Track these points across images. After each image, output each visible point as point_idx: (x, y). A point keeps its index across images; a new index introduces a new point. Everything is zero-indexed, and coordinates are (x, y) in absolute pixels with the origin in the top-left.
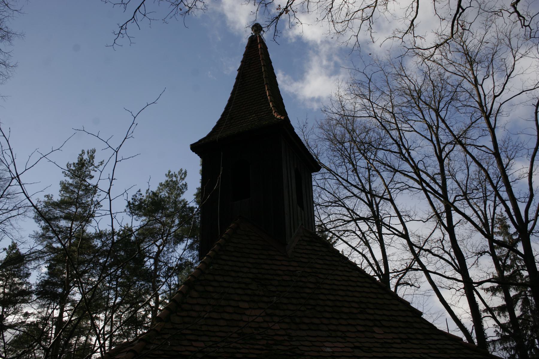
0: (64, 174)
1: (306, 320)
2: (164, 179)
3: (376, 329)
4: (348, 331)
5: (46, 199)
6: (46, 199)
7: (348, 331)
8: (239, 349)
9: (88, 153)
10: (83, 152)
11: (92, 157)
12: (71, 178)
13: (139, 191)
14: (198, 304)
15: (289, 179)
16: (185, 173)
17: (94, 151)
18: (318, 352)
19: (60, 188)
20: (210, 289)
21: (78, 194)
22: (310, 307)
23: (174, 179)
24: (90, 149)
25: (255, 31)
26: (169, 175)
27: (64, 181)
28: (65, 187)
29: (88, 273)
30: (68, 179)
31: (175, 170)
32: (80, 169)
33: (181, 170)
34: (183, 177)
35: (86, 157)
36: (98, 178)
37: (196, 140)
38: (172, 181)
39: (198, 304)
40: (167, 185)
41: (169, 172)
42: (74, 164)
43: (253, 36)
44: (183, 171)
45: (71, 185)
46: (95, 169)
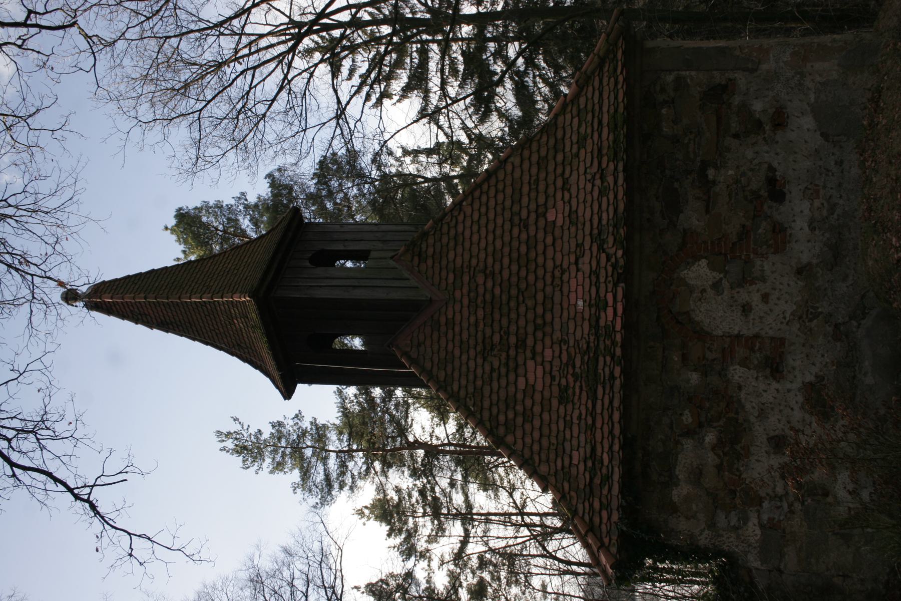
0: (260, 472)
1: (540, 310)
3: (551, 217)
5: (299, 491)
6: (299, 491)
7: (553, 259)
8: (580, 414)
9: (223, 441)
10: (223, 449)
11: (228, 435)
12: (264, 460)
15: (335, 282)
17: (219, 433)
18: (583, 319)
20: (502, 418)
22: (521, 298)
25: (76, 300)
27: (269, 470)
28: (279, 466)
29: (383, 400)
30: (265, 465)
32: (250, 451)
35: (230, 444)
37: (277, 392)
42: (244, 461)
43: (86, 306)
45: (274, 459)
46: (245, 427)
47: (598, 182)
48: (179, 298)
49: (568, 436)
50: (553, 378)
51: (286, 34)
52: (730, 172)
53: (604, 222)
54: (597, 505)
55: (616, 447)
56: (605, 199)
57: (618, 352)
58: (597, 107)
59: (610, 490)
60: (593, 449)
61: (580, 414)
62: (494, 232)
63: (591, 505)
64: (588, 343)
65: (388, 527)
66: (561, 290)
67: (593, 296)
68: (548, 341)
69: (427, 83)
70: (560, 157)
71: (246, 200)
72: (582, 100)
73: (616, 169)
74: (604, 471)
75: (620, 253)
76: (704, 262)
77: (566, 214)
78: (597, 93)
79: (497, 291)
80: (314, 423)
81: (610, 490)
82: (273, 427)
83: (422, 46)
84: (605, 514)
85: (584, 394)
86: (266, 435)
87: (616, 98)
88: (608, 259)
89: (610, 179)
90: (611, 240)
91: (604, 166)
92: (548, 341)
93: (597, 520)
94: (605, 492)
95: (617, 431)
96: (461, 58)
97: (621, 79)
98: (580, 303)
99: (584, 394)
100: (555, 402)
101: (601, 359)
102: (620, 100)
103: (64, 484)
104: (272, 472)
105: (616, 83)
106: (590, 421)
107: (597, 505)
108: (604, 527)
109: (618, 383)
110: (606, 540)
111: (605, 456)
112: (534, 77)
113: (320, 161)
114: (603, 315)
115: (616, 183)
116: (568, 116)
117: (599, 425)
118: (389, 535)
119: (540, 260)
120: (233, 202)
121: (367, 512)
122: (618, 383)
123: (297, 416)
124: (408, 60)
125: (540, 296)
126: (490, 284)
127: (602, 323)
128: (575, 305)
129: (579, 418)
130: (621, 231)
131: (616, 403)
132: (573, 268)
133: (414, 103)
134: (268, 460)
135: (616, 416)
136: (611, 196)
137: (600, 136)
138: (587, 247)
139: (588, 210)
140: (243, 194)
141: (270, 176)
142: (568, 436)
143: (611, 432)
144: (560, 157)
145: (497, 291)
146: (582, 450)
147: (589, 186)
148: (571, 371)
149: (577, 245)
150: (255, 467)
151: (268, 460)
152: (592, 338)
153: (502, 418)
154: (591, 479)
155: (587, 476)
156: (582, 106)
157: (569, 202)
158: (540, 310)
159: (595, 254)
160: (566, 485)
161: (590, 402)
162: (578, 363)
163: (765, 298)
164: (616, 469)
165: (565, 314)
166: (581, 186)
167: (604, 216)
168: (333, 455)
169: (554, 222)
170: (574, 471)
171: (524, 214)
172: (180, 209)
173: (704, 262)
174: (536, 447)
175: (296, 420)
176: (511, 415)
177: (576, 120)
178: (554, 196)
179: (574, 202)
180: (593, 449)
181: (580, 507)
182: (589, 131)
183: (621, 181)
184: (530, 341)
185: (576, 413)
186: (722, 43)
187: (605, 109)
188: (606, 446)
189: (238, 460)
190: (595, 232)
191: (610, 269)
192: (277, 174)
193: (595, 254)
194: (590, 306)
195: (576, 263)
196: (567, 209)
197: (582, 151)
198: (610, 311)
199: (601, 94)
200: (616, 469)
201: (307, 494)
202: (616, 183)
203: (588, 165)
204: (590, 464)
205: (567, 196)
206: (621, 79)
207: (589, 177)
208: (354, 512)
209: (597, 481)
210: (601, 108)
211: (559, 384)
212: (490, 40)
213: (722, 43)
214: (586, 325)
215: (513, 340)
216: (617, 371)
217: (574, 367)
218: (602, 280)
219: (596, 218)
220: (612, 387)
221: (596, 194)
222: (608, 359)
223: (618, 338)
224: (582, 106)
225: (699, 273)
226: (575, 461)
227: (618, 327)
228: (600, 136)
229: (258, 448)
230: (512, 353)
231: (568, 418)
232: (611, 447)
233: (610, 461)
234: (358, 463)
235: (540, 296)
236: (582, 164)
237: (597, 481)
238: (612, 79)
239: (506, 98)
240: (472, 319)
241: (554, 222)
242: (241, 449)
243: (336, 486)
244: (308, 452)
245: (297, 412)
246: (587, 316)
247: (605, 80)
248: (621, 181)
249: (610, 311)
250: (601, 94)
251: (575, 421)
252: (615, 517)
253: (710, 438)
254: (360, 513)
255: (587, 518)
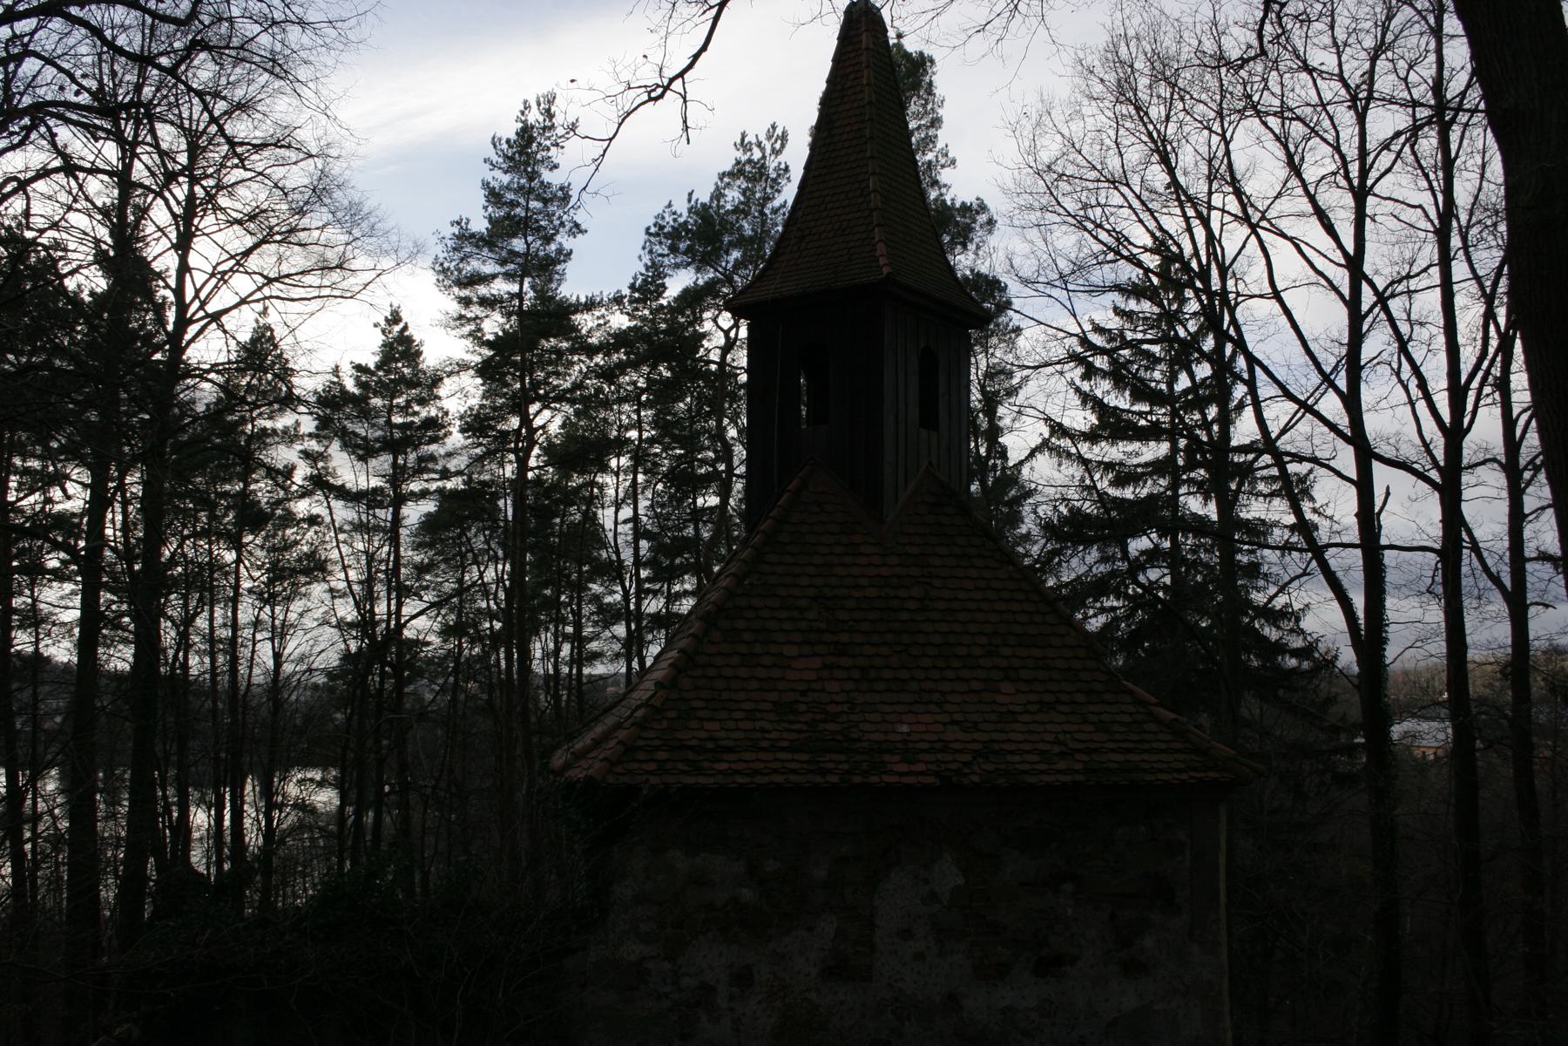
0: (488, 166)
1: (887, 674)
2: (728, 158)
3: (1006, 687)
4: (953, 691)
5: (456, 230)
7: (953, 691)
8: (768, 732)
9: (539, 104)
10: (527, 106)
11: (549, 114)
12: (506, 172)
13: (670, 205)
14: (719, 654)
16: (784, 138)
17: (551, 102)
18: (886, 733)
19: (483, 201)
20: (741, 624)
21: (522, 210)
23: (757, 154)
24: (544, 90)
26: (744, 145)
28: (494, 196)
30: (498, 174)
31: (757, 130)
33: (774, 127)
34: (778, 146)
35: (534, 117)
36: (567, 165)
38: (750, 161)
39: (719, 654)
40: (738, 172)
41: (743, 136)
44: (779, 131)
47: (1056, 749)
48: (873, 157)
49: (736, 715)
50: (804, 693)
51: (1208, 255)
52: (1070, 911)
53: (1009, 758)
54: (661, 755)
55: (740, 780)
56: (1035, 758)
57: (857, 779)
58: (1147, 746)
59: (683, 772)
60: (729, 750)
61: (768, 732)
62: (980, 610)
63: (658, 748)
64: (858, 740)
65: (372, 366)
66: (915, 702)
67: (919, 746)
68: (850, 685)
69: (1106, 439)
70: (1080, 698)
71: (943, 166)
72: (1153, 727)
73: (1076, 771)
74: (706, 764)
75: (976, 779)
76: (961, 881)
77: (1011, 708)
78: (1164, 746)
79: (904, 616)
80: (564, 255)
81: (683, 772)
82: (562, 189)
83: (1165, 431)
84: (652, 766)
85: (795, 736)
86: (547, 176)
87: (1161, 771)
88: (966, 764)
89: (1062, 765)
90: (990, 767)
91: (1078, 756)
92: (850, 685)
93: (641, 756)
94: (680, 766)
95: (759, 780)
96: (1144, 493)
97: (1184, 776)
98: (905, 729)
99: (795, 736)
100: (773, 696)
101: (842, 757)
102: (1160, 776)
103: (690, 66)
104: (486, 185)
105: (1179, 771)
106: (764, 744)
107: (661, 755)
108: (635, 766)
109: (819, 779)
110: (619, 769)
111: (723, 766)
112: (1113, 609)
113: (999, 282)
114: (897, 758)
115: (1059, 772)
116: (1132, 709)
117: (762, 756)
118: (359, 368)
119: (950, 674)
120: (940, 145)
121: (397, 328)
122: (819, 779)
123: (577, 225)
124: (1146, 408)
125: (904, 674)
126: (912, 605)
127: (886, 757)
128: (901, 722)
129: (763, 730)
130: (1002, 781)
131: (793, 778)
132: (945, 718)
133: (1081, 419)
134: (506, 179)
135: (779, 779)
136: (1042, 767)
137: (1113, 750)
138: (976, 736)
139: (1020, 737)
140: (953, 162)
141: (983, 208)
142: (736, 715)
143: (756, 772)
144: (1080, 698)
145: (904, 616)
146: (723, 734)
147: (1050, 738)
148: (818, 717)
149: (975, 723)
150: (495, 159)
151: (506, 179)
152: (865, 745)
153: (741, 624)
154: (691, 748)
155: (694, 743)
156: (1145, 726)
157: (1027, 712)
158: (887, 674)
159: (970, 746)
160: (672, 714)
161: (786, 744)
162: (831, 727)
163: (919, 957)
164: (711, 780)
165: (887, 708)
166: (1048, 727)
167: (1017, 758)
168: (515, 288)
169: (999, 692)
170: (694, 724)
171: (1006, 651)
172: (932, 61)
173: (961, 881)
174: (711, 672)
175: (568, 226)
176: (747, 636)
177: (1127, 719)
178: (1031, 691)
179: (1027, 718)
180: (729, 750)
181: (652, 734)
182: (1118, 737)
183: (1062, 778)
184: (845, 661)
185: (768, 726)
186: (1223, 898)
187: (1146, 757)
188: (739, 766)
189: (510, 130)
190: (996, 747)
191: (954, 766)
192: (982, 218)
193: (970, 746)
194: (905, 741)
195: (953, 722)
196: (1018, 709)
197: (1091, 728)
198: (904, 768)
199: (1163, 751)
200: (711, 780)
201: (450, 243)
202: (1059, 772)
203: (1076, 736)
204: (710, 745)
205: (1033, 708)
206: (1184, 776)
207: (1061, 737)
208: (395, 305)
209: (691, 755)
210: (1146, 751)
211: (797, 702)
212: (1174, 541)
213: (1223, 898)
214: (881, 737)
215: (845, 638)
216: (834, 779)
217: (824, 721)
218: (939, 756)
219: (1013, 747)
220: (811, 772)
221: (1041, 746)
222: (846, 767)
223: (874, 779)
224: (1145, 726)
225: (948, 875)
226: (707, 725)
227: (886, 778)
228: (1113, 750)
229: (527, 164)
230: (827, 637)
231: (759, 715)
232: (737, 772)
233: (720, 772)
234: (493, 324)
235: (904, 674)
236: (1075, 727)
237: (691, 755)
238: (1182, 766)
239: (1080, 564)
240: (863, 581)
241: (999, 692)
242: (526, 135)
243: (465, 293)
244: (518, 244)
245: (583, 227)
246: (891, 737)
247: (1181, 757)
248: (1062, 778)
249: (904, 768)
250: (1163, 751)
251: (758, 725)
252: (654, 780)
253: (747, 894)
254: (395, 318)
255: (641, 743)
